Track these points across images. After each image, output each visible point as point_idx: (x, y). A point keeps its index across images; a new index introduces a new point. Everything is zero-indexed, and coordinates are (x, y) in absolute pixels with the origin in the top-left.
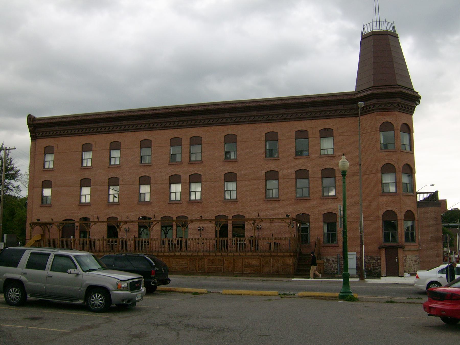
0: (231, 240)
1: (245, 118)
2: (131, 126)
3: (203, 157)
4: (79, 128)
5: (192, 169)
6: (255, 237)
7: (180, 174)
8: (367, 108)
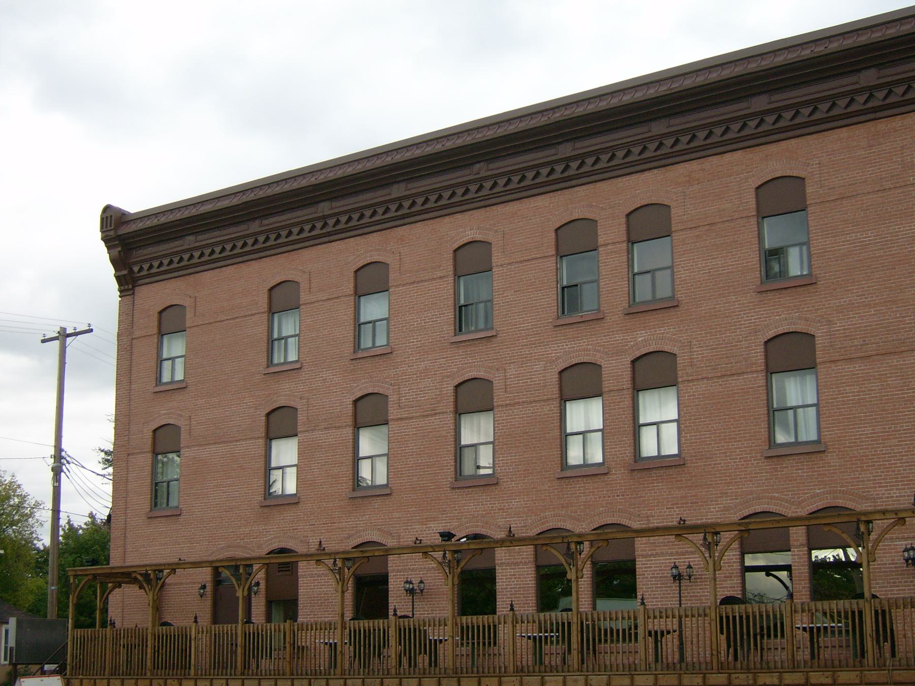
0: (534, 622)
1: (890, 92)
2: (590, 161)
3: (677, 282)
4: (483, 174)
5: (641, 336)
6: (874, 596)
7: (597, 358)
8: (245, 242)
